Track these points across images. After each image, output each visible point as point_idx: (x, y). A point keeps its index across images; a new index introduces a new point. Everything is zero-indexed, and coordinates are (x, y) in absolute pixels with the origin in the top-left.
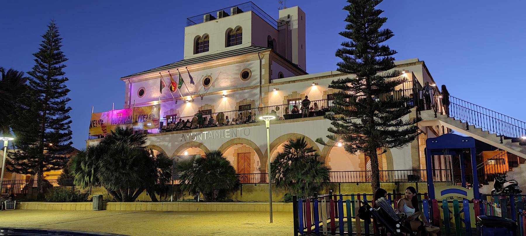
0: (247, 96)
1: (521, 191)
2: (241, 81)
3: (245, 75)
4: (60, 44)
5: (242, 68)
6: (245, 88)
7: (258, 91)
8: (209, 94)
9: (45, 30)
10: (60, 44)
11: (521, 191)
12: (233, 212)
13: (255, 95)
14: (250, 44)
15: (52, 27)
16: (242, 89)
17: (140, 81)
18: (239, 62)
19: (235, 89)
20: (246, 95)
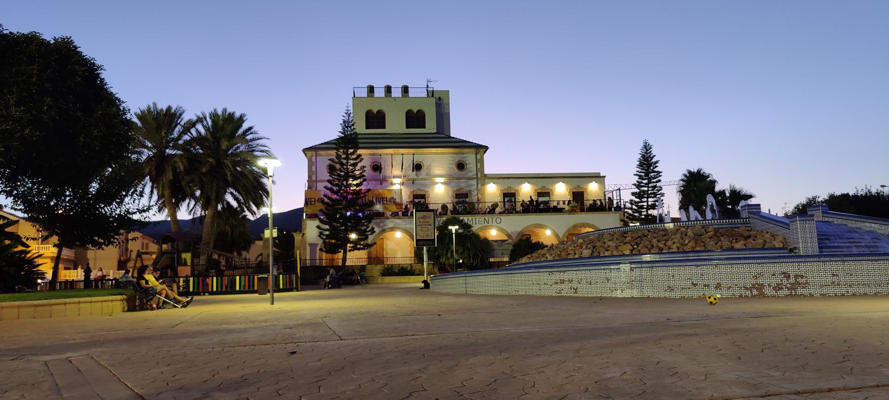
0: (463, 184)
1: (750, 197)
2: (456, 170)
3: (461, 166)
4: (654, 160)
5: (457, 158)
6: (461, 179)
7: (474, 182)
8: (422, 179)
9: (642, 145)
10: (654, 160)
11: (750, 197)
12: (253, 322)
13: (472, 185)
14: (435, 131)
15: (647, 148)
16: (458, 179)
17: (422, 154)
18: (454, 153)
19: (451, 179)
20: (463, 185)
